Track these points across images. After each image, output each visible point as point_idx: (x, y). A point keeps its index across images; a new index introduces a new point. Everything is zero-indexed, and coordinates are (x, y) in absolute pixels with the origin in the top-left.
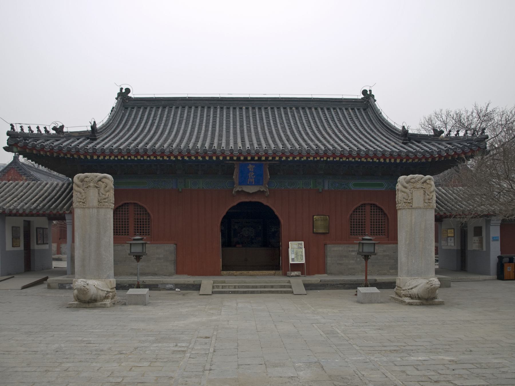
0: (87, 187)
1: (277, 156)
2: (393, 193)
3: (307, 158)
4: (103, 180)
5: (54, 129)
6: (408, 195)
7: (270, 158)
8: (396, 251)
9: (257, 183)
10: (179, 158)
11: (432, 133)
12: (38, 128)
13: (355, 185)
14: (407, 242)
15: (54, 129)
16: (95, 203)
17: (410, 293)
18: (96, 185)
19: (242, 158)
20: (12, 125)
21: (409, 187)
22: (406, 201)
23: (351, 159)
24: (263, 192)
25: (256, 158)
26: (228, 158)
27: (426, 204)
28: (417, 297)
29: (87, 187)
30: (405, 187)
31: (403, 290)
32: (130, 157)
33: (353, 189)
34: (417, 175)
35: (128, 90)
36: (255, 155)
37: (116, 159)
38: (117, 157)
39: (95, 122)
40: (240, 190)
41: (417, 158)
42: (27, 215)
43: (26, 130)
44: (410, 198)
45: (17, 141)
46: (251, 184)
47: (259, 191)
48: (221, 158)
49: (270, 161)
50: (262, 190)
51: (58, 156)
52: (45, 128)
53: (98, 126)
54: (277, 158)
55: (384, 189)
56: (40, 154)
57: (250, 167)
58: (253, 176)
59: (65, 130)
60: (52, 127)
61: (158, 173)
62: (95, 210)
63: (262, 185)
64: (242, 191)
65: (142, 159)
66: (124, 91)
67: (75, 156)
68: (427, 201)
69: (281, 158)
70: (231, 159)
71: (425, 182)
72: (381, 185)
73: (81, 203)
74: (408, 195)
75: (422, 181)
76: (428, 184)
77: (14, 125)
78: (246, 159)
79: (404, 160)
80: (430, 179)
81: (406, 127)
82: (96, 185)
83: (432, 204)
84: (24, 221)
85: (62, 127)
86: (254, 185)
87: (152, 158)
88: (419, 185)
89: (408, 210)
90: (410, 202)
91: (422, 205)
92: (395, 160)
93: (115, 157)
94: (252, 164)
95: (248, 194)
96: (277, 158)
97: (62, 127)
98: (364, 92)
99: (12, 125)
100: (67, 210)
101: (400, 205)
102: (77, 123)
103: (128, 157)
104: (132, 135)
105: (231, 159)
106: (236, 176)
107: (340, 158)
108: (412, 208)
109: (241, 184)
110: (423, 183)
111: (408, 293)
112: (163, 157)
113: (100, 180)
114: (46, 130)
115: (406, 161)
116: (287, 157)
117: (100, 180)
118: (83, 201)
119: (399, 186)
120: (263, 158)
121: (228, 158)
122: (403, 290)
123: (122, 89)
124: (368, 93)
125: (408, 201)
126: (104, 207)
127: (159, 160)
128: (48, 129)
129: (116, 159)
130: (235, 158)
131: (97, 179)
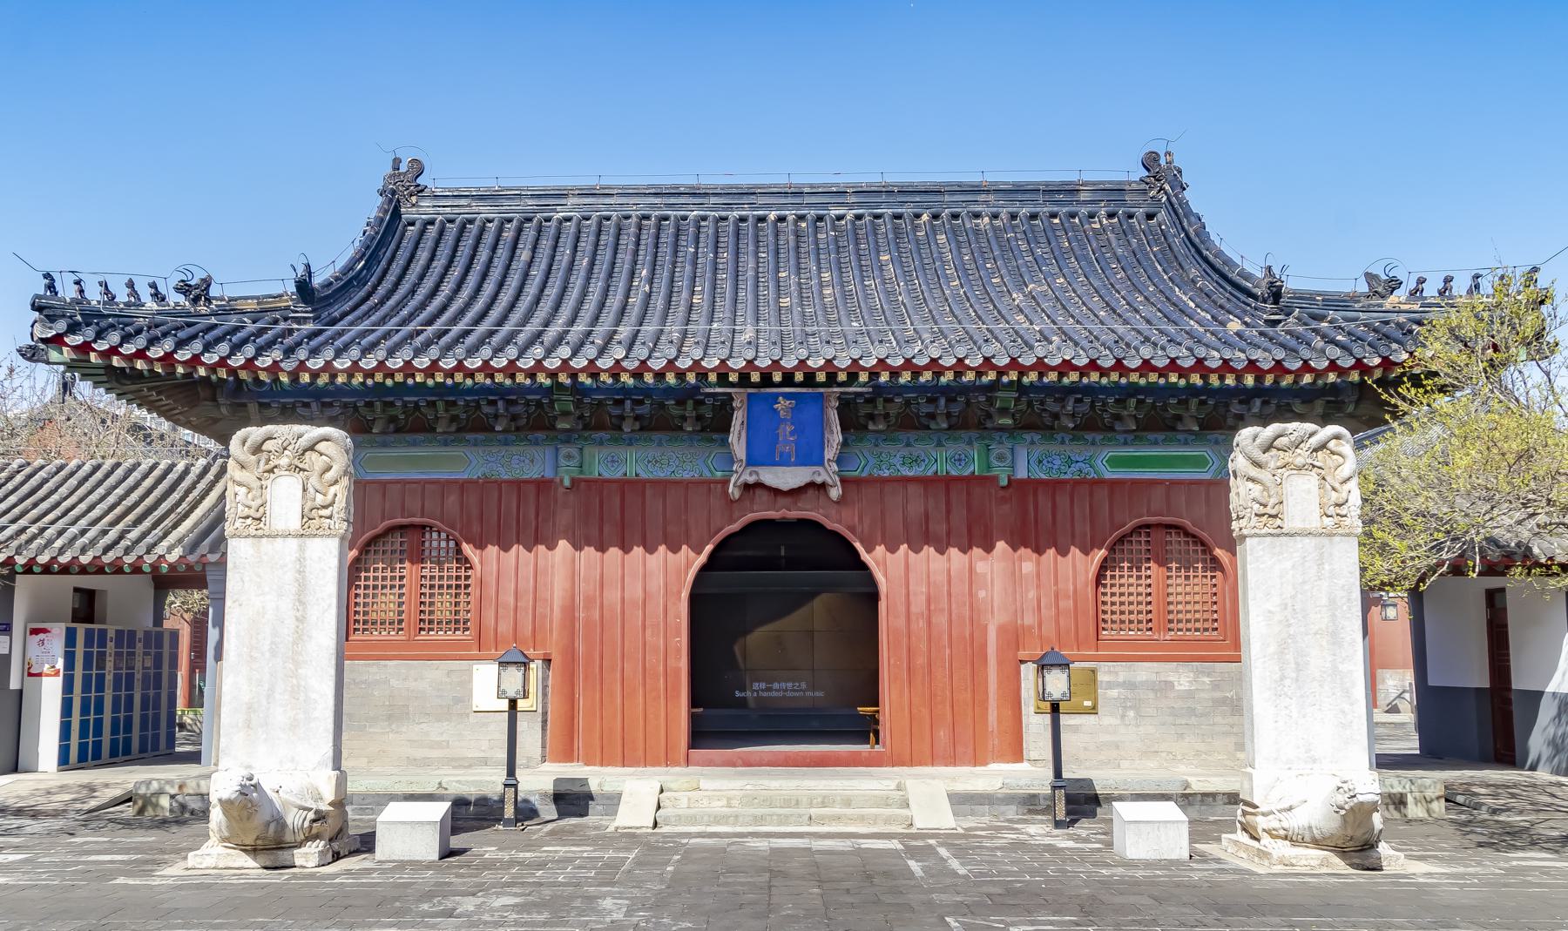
0: (271, 471)
1: (864, 369)
2: (1219, 487)
3: (958, 374)
4: (321, 447)
5: (184, 288)
6: (1266, 489)
7: (842, 377)
8: (1241, 681)
9: (811, 456)
10: (563, 378)
11: (1363, 288)
12: (131, 285)
13: (1115, 462)
14: (1272, 649)
15: (184, 288)
16: (295, 523)
17: (1285, 825)
18: (296, 462)
19: (755, 377)
20: (47, 276)
21: (1272, 465)
22: (1262, 510)
23: (1173, 378)
24: (823, 487)
25: (799, 377)
26: (713, 377)
27: (1327, 521)
28: (1307, 838)
29: (271, 471)
30: (1257, 464)
31: (1264, 814)
32: (413, 376)
33: (1108, 476)
34: (1295, 425)
35: (418, 168)
36: (796, 368)
37: (370, 382)
38: (372, 376)
39: (308, 266)
40: (751, 480)
41: (1310, 370)
42: (84, 570)
43: (94, 296)
44: (1272, 501)
45: (84, 335)
46: (784, 462)
47: (811, 485)
48: (691, 378)
49: (754, 385)
50: (819, 480)
51: (186, 375)
52: (153, 286)
53: (317, 281)
54: (863, 377)
55: (1207, 476)
56: (133, 369)
57: (782, 405)
58: (792, 433)
59: (214, 291)
60: (174, 280)
61: (498, 428)
62: (293, 543)
63: (821, 464)
64: (759, 485)
65: (449, 381)
66: (403, 168)
67: (243, 375)
68: (1331, 510)
69: (874, 374)
70: (723, 378)
71: (1323, 446)
72: (1199, 462)
73: (249, 521)
74: (1266, 489)
75: (1314, 441)
76: (1333, 453)
77: (56, 276)
78: (766, 379)
79: (1269, 380)
80: (1337, 437)
81: (1276, 271)
82: (296, 462)
83: (1347, 521)
84: (76, 590)
85: (207, 282)
86: (796, 464)
87: (480, 378)
88: (1302, 456)
89: (1269, 539)
90: (1273, 512)
91: (1314, 522)
92: (1239, 378)
93: (446, 376)
94: (787, 396)
95: (776, 492)
96: (863, 377)
97: (207, 282)
98: (1150, 162)
99: (47, 276)
100: (211, 551)
101: (1243, 523)
102: (255, 274)
103: (406, 377)
104: (423, 306)
105: (723, 378)
106: (737, 441)
107: (1061, 375)
108: (1280, 533)
109: (752, 461)
110: (1315, 450)
111: (1276, 825)
112: (513, 376)
113: (312, 448)
114: (158, 296)
115: (1276, 382)
116: (1239, 377)
117: (312, 448)
118: (258, 515)
119: (1238, 462)
120: (821, 377)
121: (713, 377)
122: (1264, 814)
123: (397, 163)
124: (1163, 162)
125: (1269, 510)
126: (320, 532)
127: (501, 384)
128: (162, 290)
129: (370, 382)
130: (733, 378)
131: (303, 442)
